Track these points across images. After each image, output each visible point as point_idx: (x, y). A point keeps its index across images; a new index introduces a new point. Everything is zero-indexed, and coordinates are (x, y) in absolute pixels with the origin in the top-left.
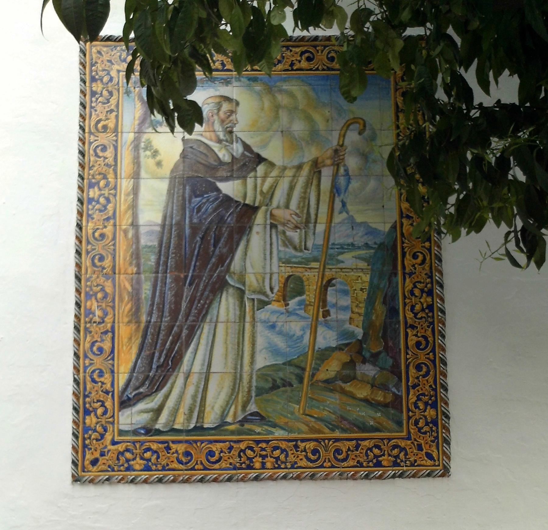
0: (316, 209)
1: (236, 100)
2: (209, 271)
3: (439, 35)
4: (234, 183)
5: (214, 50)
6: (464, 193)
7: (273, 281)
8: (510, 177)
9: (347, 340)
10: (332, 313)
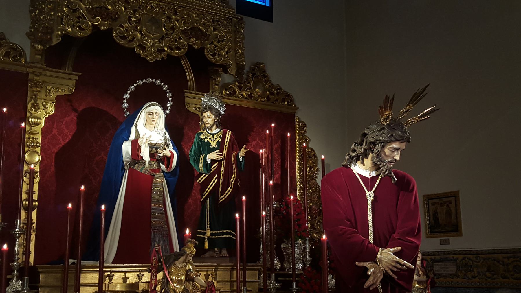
4: (187, 97)
5: (360, 261)
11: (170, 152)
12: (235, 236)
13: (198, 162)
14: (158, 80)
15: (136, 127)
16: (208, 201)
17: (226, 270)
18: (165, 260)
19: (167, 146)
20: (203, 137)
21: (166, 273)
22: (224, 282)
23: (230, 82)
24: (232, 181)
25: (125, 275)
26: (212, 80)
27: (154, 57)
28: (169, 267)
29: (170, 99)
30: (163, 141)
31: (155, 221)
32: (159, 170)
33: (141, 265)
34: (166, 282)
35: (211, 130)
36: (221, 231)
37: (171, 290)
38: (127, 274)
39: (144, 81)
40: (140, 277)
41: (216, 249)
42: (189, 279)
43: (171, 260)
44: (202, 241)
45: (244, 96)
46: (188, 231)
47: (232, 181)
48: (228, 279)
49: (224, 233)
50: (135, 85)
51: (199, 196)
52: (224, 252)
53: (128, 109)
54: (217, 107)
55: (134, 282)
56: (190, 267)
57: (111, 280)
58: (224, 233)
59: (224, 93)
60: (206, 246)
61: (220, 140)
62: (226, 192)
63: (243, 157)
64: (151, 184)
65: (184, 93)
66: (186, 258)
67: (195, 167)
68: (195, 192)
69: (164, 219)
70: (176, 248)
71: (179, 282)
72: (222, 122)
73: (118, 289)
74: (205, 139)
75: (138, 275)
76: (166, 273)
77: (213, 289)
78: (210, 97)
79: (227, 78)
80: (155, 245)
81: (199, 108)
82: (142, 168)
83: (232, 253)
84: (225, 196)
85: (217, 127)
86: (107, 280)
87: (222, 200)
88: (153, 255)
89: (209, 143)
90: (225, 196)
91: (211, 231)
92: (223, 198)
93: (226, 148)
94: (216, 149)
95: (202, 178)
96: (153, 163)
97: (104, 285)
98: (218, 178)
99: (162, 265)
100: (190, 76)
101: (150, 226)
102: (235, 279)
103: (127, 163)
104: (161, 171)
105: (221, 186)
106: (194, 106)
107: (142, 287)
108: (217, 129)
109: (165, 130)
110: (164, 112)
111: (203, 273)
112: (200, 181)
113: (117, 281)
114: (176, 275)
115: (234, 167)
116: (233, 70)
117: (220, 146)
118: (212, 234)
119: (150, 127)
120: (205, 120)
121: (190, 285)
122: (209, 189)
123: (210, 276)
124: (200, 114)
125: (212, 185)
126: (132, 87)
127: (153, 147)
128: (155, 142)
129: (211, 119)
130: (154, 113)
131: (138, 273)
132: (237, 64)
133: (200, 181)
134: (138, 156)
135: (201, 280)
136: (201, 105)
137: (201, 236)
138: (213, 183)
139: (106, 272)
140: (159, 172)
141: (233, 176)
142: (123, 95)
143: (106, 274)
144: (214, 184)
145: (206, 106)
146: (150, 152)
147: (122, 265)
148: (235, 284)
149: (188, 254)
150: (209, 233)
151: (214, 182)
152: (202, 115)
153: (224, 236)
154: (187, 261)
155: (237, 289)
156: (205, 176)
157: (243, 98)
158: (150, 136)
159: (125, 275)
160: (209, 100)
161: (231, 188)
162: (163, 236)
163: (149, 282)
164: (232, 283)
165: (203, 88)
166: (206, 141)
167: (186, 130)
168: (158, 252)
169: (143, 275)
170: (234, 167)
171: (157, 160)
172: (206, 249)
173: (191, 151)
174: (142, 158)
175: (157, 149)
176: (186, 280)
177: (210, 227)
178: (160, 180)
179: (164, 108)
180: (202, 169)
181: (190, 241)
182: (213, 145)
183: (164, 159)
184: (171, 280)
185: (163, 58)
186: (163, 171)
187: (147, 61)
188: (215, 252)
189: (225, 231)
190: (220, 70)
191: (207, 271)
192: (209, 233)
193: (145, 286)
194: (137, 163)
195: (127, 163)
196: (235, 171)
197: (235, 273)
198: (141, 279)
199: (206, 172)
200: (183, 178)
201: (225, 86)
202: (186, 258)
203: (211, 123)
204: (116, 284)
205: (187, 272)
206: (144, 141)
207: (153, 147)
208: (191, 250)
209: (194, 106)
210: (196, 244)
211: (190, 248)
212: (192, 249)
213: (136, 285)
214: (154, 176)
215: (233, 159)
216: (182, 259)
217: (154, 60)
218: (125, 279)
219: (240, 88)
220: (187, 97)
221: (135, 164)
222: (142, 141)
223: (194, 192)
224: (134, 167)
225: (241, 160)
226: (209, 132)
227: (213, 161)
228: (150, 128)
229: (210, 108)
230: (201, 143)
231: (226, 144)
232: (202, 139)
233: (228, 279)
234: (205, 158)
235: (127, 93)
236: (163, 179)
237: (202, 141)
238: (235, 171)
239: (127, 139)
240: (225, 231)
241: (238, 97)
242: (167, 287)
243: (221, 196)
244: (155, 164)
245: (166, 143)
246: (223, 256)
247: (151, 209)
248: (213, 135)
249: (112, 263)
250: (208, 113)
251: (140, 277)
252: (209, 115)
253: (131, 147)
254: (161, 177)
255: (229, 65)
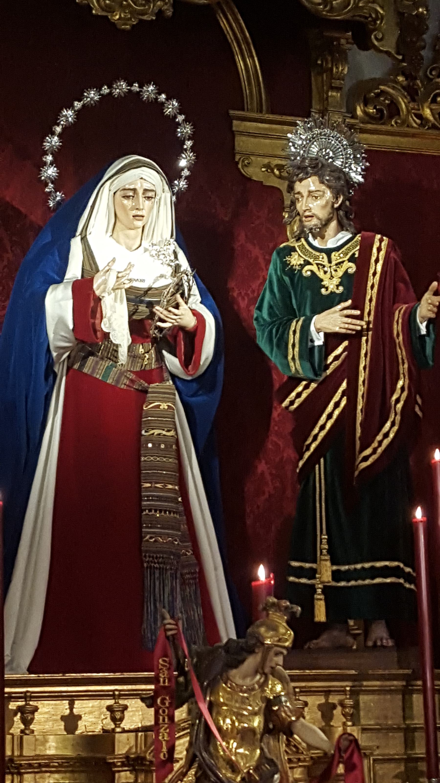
0: (94, 258)
1: (121, 244)
2: (155, 361)
3: (267, 171)
4: (242, 133)
6: (431, 363)
7: (297, 365)
8: (341, 288)
9: (220, 359)
10: (330, 573)
11: (195, 313)
12: (416, 580)
13: (282, 345)
14: (149, 83)
15: (84, 239)
16: (320, 470)
17: (390, 692)
18: (196, 667)
19: (182, 295)
20: (295, 260)
21: (204, 707)
22: (383, 730)
23: (378, 74)
24: (398, 401)
25: (71, 707)
26: (320, 74)
27: (133, 13)
28: (211, 687)
29: (189, 144)
30: (169, 281)
31: (154, 537)
32: (160, 372)
33: (118, 675)
34: (204, 738)
35: (323, 237)
36: (367, 565)
37: (221, 763)
38: (77, 704)
39: (105, 90)
40: (116, 714)
41: (351, 623)
42: (277, 726)
43: (219, 666)
44: (305, 597)
45: (427, 120)
46: (262, 573)
47: (398, 401)
48: (395, 720)
49: (376, 572)
50: (78, 105)
51: (290, 453)
52: (380, 632)
53: (58, 182)
54: (338, 163)
55: (98, 729)
56: (279, 688)
57: (27, 722)
58: (376, 572)
59: (359, 112)
60: (321, 614)
61: (352, 268)
62: (379, 438)
63: (430, 321)
64: (137, 420)
65: (230, 120)
66: (264, 660)
67: (274, 358)
68: (278, 438)
69: (184, 527)
70: (227, 629)
71: (246, 736)
72: (359, 210)
73: (51, 752)
74: (302, 266)
75: (109, 708)
76: (204, 707)
77: (356, 758)
78: (317, 131)
79: (368, 65)
80: (163, 618)
81: (280, 167)
82: (109, 368)
83: (405, 636)
84: (375, 451)
85: (341, 227)
86: (17, 726)
87: (364, 465)
88: (158, 650)
89: (315, 281)
90: (375, 451)
91: (333, 563)
92: (368, 458)
93: (372, 293)
94: (342, 298)
95: (299, 395)
96: (141, 350)
97: (8, 737)
98: (352, 393)
99: (188, 682)
100: (247, 64)
101: (140, 551)
102: (418, 720)
103: (60, 356)
104: (166, 375)
105: (359, 417)
106: (266, 161)
107: (123, 745)
108: (340, 235)
109: (174, 246)
110: (171, 185)
111: (315, 701)
112: (292, 403)
113: (48, 726)
114: (235, 714)
115: (402, 353)
116: (387, 37)
117: (354, 287)
118: (337, 576)
119: (127, 236)
120: (300, 206)
121: (280, 747)
122: (323, 427)
123: (338, 711)
124: (283, 186)
125: (330, 416)
126: (70, 113)
127: (138, 299)
128: (144, 285)
129: (321, 202)
130: (140, 192)
131: (110, 702)
132: (401, 15)
133: (292, 403)
134: (95, 331)
135: (311, 730)
136: (287, 158)
137: (303, 581)
138: (333, 411)
139: (11, 697)
140: (162, 380)
141: (400, 383)
142: (42, 140)
143: (13, 706)
144: (337, 412)
145: (303, 159)
146: (130, 316)
147: (58, 676)
148: (420, 737)
149: (269, 648)
150: (326, 570)
151: (337, 405)
152: (291, 188)
153: (378, 580)
154: (267, 670)
155: (428, 752)
156: (306, 387)
157: (422, 125)
158: (130, 266)
159: (71, 707)
160: (311, 141)
161: (393, 424)
162: (183, 583)
163: (145, 729)
164: (408, 732)
165: (292, 100)
166: (306, 272)
167: (241, 238)
168: (173, 640)
169: (126, 707)
170: (402, 353)
171: (155, 341)
172: (320, 623)
173: (260, 308)
174: (106, 336)
175: (150, 305)
176: (267, 730)
177: (329, 552)
178: (164, 406)
179: (171, 174)
180: (296, 366)
181: (273, 604)
182: (331, 284)
183: (175, 337)
184: (220, 729)
185: (160, 13)
186: (174, 377)
187: (113, 25)
188: (348, 631)
189: (379, 564)
190: (345, 39)
191: (327, 693)
192: (326, 570)
193: (132, 742)
194: (92, 354)
195: (60, 356)
196: (404, 368)
197: (417, 700)
198: (121, 719)
199: (311, 375)
200: (236, 396)
201: (363, 92)
202: (264, 660)
203: (323, 214)
204: (45, 734)
205: (269, 703)
206: (112, 282)
207: (138, 299)
208: (278, 633)
209: (266, 161)
210: (293, 615)
211: (275, 629)
212: (282, 630)
213: (106, 739)
214: (145, 392)
215: (397, 328)
216: (251, 662)
217: (134, 22)
218: (71, 721)
219: (412, 93)
220: (242, 133)
221: (85, 358)
222: (105, 282)
223: (275, 439)
224: (82, 366)
225: (424, 331)
226: (316, 243)
227: (332, 339)
228: (128, 242)
229: (317, 167)
230: (292, 280)
231: (374, 280)
232: (292, 269)
233: (395, 720)
234: (305, 328)
235: (53, 133)
236: (175, 403)
237: (292, 273)
238: (404, 368)
239: (59, 279)
240: (379, 564)
241: (405, 123)
242: (207, 751)
243: (363, 449)
244: (147, 354)
245: (179, 286)
246: (375, 645)
247: (140, 499)
248: (329, 252)
249: (30, 670)
250: (311, 184)
251: (116, 714)
252: (313, 188)
253: (70, 303)
254: (165, 396)
255: (375, 20)
